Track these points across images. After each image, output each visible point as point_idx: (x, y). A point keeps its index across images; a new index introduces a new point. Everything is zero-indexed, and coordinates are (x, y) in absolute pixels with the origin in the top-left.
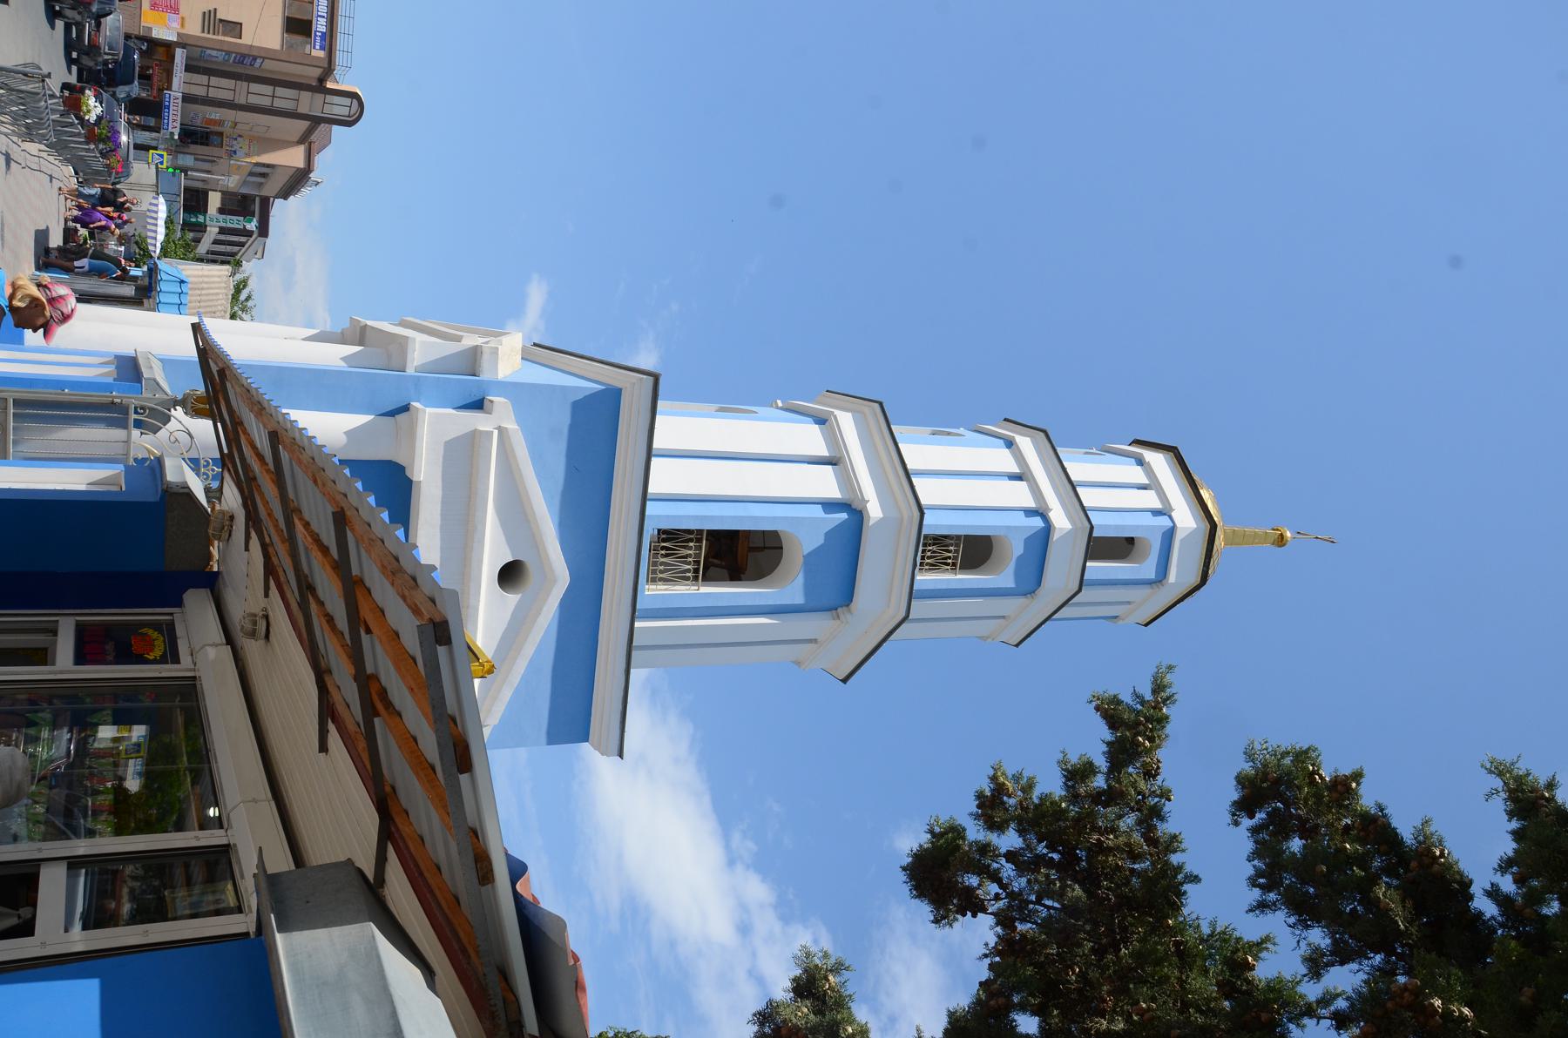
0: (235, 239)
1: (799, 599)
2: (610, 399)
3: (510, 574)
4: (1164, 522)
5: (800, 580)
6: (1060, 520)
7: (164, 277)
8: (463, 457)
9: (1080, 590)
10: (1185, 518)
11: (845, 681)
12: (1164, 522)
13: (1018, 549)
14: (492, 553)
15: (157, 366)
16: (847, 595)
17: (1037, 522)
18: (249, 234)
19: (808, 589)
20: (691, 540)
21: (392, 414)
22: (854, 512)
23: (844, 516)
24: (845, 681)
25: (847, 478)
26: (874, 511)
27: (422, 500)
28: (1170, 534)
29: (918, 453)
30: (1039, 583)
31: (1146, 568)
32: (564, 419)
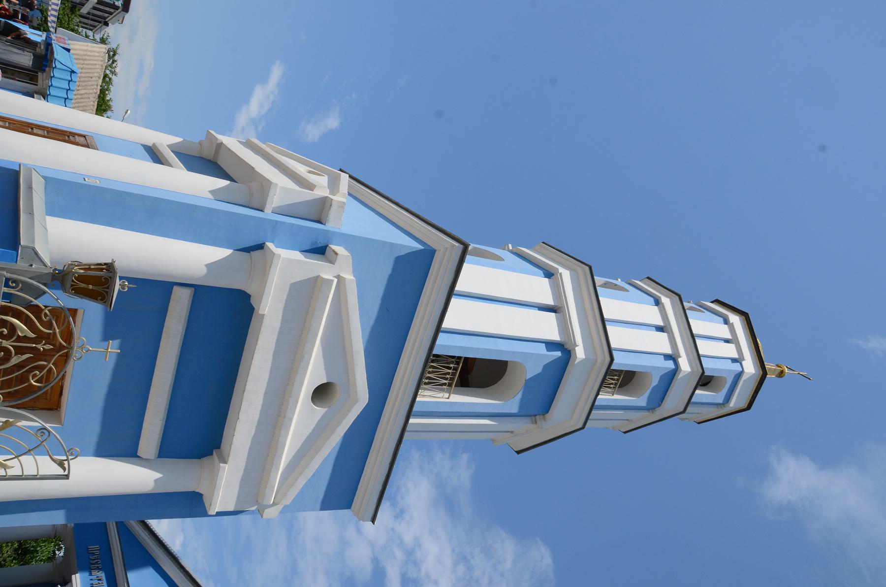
0: (107, 9)
1: (515, 410)
2: (427, 255)
3: (321, 393)
4: (736, 367)
5: (519, 396)
6: (685, 365)
7: (58, 65)
8: (305, 294)
9: (684, 411)
10: (750, 367)
11: (518, 452)
12: (736, 367)
13: (655, 381)
14: (313, 374)
15: (38, 185)
16: (546, 407)
17: (670, 365)
18: (117, 8)
19: (522, 405)
20: (452, 363)
21: (248, 250)
22: (564, 349)
23: (558, 354)
24: (518, 452)
25: (564, 325)
26: (580, 352)
27: (263, 329)
28: (739, 375)
29: (612, 307)
30: (660, 405)
31: (718, 397)
32: (386, 269)
